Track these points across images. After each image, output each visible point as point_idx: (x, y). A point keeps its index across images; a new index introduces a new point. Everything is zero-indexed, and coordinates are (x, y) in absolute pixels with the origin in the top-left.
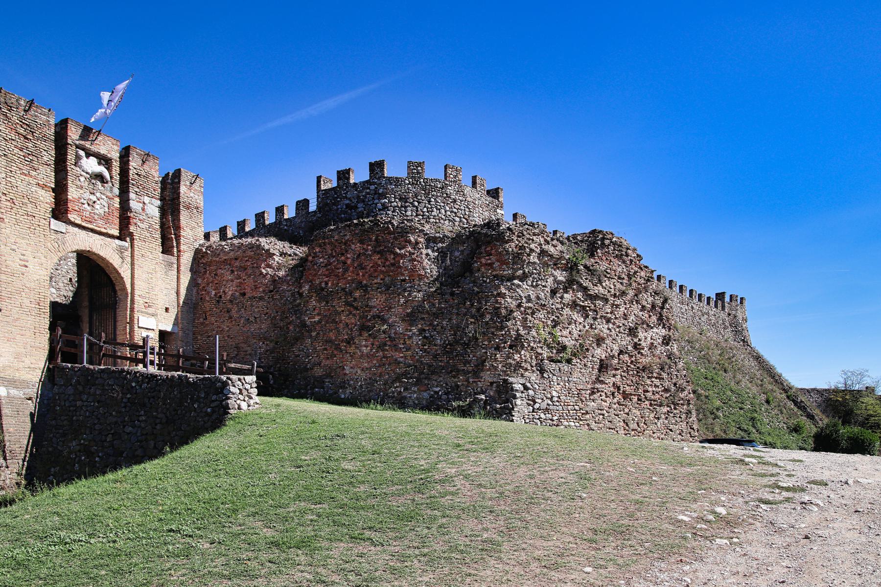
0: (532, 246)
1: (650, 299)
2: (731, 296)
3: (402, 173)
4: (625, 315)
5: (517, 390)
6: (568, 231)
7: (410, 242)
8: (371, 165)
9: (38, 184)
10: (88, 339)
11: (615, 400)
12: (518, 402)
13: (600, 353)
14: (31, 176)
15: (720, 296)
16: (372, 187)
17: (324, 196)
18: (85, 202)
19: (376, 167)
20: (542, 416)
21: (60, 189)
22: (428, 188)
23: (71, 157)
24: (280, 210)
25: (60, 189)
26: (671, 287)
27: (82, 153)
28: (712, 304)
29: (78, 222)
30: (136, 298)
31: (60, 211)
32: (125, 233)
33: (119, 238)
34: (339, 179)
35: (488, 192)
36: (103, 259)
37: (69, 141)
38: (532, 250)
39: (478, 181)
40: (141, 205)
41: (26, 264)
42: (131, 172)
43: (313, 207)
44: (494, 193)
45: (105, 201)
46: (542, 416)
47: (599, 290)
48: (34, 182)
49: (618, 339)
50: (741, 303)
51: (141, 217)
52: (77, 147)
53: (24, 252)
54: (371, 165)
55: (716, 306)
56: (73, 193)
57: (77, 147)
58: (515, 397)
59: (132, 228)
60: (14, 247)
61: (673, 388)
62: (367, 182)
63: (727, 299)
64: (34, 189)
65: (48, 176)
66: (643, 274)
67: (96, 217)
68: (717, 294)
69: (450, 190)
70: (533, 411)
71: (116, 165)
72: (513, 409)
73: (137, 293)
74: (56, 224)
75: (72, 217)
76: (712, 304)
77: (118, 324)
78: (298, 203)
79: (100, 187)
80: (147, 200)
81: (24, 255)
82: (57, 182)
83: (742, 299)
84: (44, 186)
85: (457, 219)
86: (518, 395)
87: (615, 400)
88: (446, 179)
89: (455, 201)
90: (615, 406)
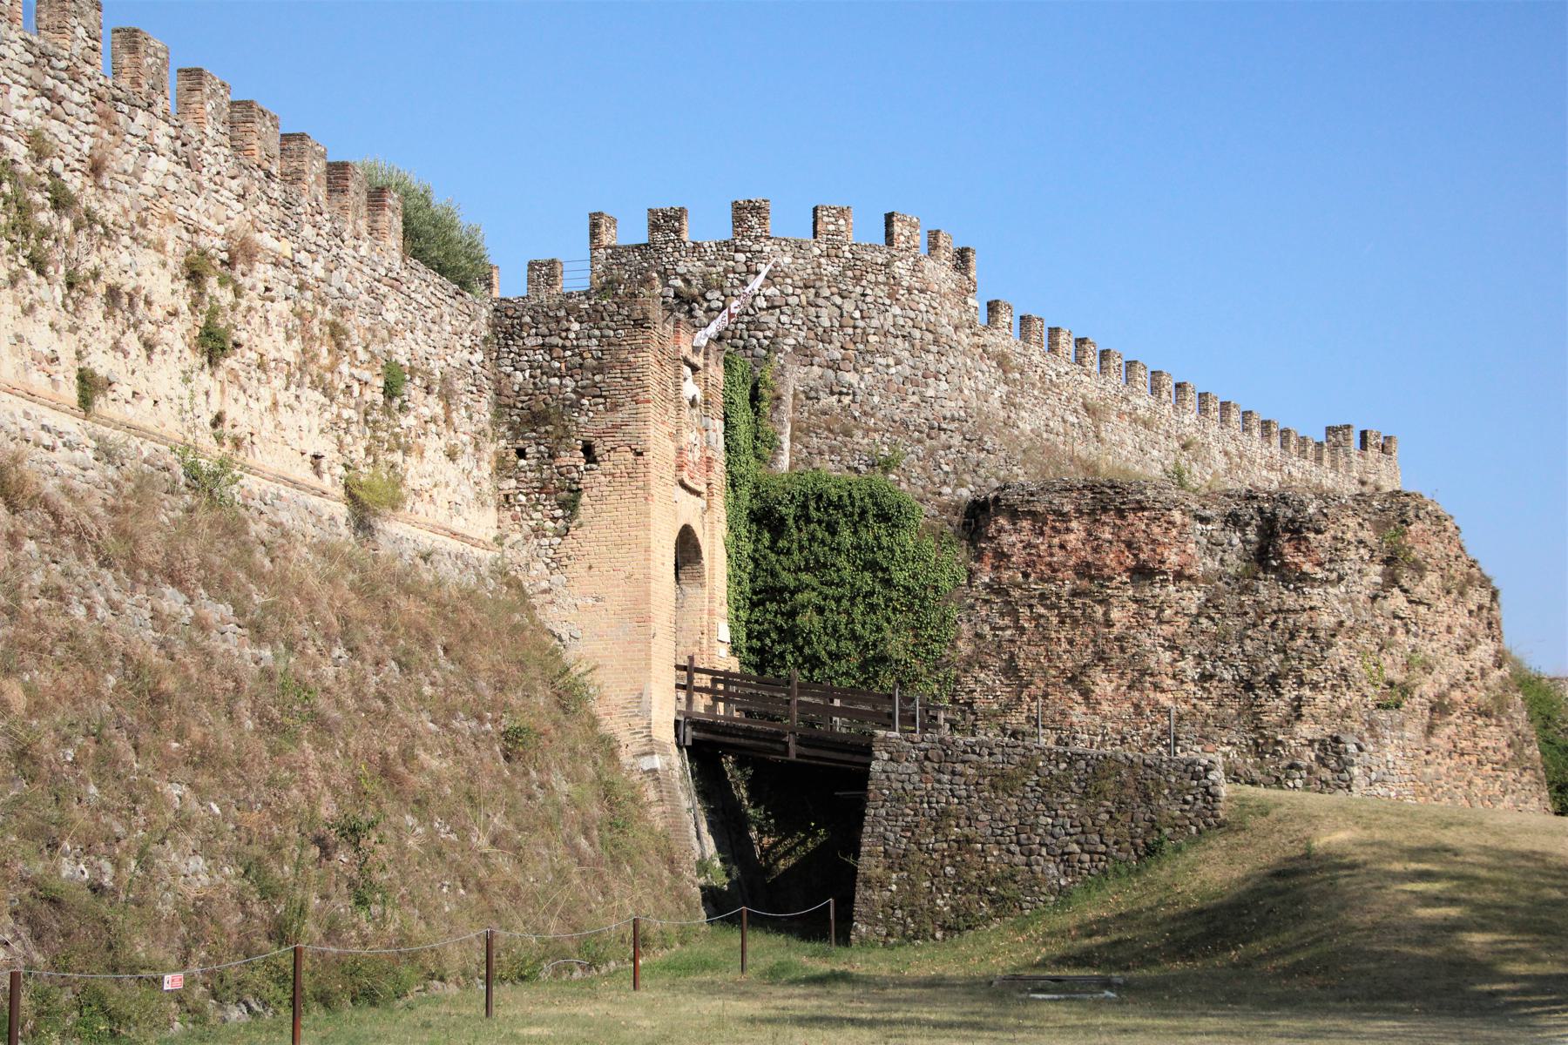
8: (737, 208)
12: (1355, 771)
13: (1428, 688)
16: (741, 257)
34: (654, 227)
44: (962, 258)
54: (737, 208)
62: (727, 244)
68: (1331, 430)
85: (917, 334)
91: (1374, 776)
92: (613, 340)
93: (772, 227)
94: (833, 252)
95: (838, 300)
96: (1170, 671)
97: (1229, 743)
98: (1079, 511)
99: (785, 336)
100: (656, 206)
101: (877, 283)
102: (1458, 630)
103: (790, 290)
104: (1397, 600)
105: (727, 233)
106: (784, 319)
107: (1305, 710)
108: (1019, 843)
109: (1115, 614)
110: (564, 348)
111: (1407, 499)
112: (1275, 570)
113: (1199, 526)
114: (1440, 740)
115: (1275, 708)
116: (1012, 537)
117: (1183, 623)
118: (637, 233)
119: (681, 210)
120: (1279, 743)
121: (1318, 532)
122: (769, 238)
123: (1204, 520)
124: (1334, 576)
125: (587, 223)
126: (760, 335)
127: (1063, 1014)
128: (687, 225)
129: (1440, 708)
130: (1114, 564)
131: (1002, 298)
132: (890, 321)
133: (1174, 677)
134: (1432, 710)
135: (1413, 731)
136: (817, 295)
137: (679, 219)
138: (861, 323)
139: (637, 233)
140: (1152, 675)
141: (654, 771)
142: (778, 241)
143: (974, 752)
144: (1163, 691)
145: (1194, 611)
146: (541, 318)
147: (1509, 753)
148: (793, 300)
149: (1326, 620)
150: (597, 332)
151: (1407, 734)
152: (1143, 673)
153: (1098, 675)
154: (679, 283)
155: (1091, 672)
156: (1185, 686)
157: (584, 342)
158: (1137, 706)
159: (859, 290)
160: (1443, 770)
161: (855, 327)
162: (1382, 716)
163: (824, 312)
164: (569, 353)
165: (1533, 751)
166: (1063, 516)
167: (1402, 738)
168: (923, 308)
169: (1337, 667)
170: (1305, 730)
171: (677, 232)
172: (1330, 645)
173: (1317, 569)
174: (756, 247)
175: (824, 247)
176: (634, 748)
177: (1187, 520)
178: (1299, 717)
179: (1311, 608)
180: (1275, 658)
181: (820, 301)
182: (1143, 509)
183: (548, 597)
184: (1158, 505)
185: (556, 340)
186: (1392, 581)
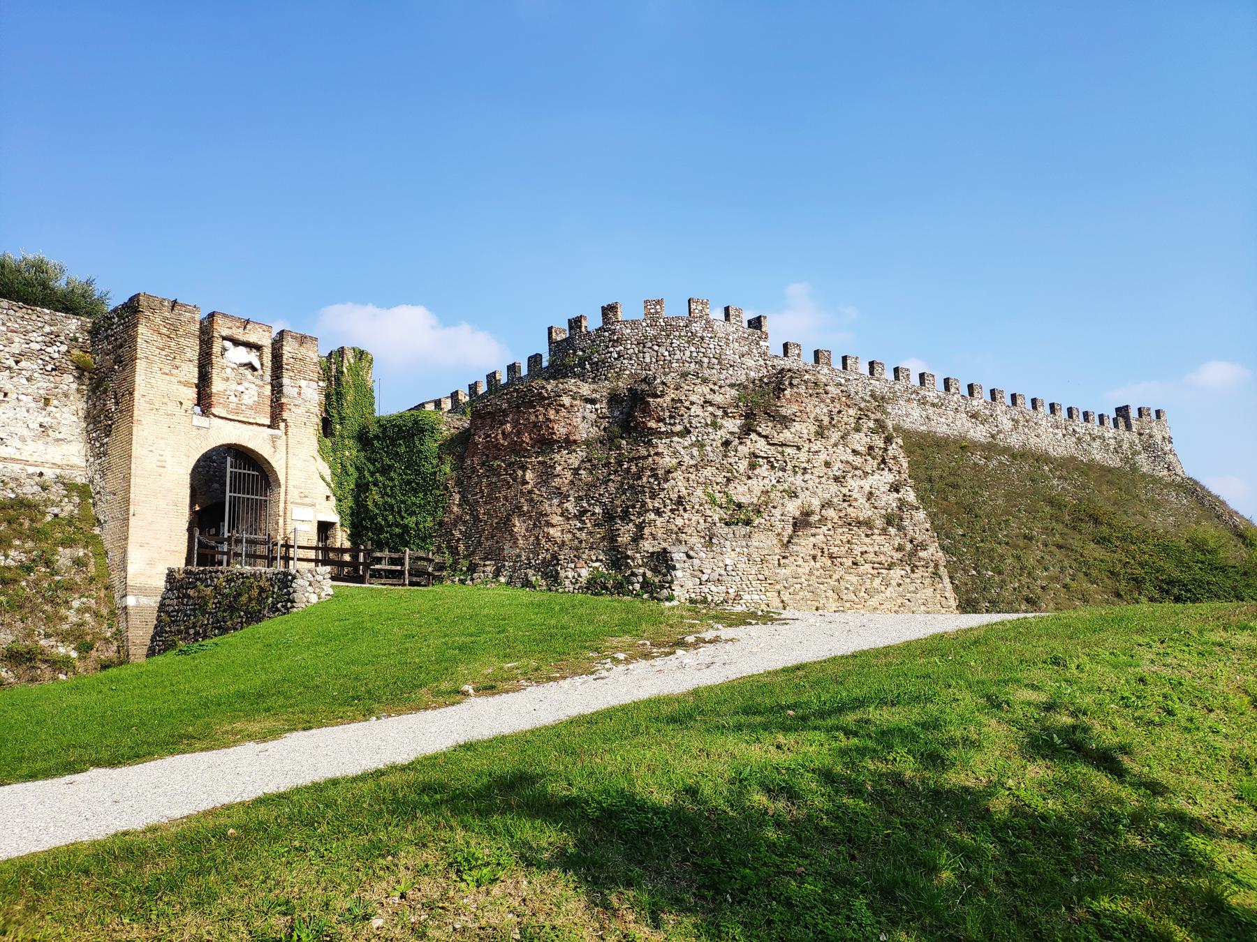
0: (693, 398)
1: (866, 440)
2: (1140, 409)
3: (639, 315)
7: (563, 406)
10: (200, 541)
11: (818, 565)
15: (1122, 412)
17: (557, 348)
19: (609, 311)
20: (713, 588)
22: (669, 328)
23: (216, 349)
26: (1034, 407)
27: (228, 344)
28: (1109, 423)
33: (269, 427)
34: (571, 328)
36: (253, 451)
37: (216, 334)
38: (692, 403)
39: (732, 312)
40: (297, 390)
42: (285, 357)
44: (756, 323)
45: (255, 391)
46: (713, 588)
47: (786, 435)
49: (819, 491)
50: (1158, 417)
52: (224, 338)
55: (1116, 426)
56: (217, 386)
57: (224, 338)
58: (674, 568)
59: (285, 415)
61: (909, 546)
63: (1133, 414)
64: (175, 387)
65: (192, 374)
66: (851, 412)
68: (1117, 410)
69: (696, 327)
71: (267, 353)
73: (291, 483)
74: (204, 421)
75: (214, 410)
76: (1109, 423)
78: (530, 359)
79: (250, 377)
80: (303, 383)
84: (186, 384)
85: (706, 360)
86: (678, 566)
87: (818, 565)
89: (702, 338)
90: (817, 573)
91: (705, 578)
93: (620, 316)
95: (656, 348)
96: (559, 511)
97: (597, 560)
107: (647, 531)
113: (589, 406)
114: (805, 544)
120: (628, 557)
121: (656, 396)
127: (381, 766)
128: (584, 323)
132: (688, 354)
133: (562, 515)
144: (553, 526)
153: (890, 529)
163: (647, 355)
172: (667, 480)
173: (661, 424)
182: (545, 398)
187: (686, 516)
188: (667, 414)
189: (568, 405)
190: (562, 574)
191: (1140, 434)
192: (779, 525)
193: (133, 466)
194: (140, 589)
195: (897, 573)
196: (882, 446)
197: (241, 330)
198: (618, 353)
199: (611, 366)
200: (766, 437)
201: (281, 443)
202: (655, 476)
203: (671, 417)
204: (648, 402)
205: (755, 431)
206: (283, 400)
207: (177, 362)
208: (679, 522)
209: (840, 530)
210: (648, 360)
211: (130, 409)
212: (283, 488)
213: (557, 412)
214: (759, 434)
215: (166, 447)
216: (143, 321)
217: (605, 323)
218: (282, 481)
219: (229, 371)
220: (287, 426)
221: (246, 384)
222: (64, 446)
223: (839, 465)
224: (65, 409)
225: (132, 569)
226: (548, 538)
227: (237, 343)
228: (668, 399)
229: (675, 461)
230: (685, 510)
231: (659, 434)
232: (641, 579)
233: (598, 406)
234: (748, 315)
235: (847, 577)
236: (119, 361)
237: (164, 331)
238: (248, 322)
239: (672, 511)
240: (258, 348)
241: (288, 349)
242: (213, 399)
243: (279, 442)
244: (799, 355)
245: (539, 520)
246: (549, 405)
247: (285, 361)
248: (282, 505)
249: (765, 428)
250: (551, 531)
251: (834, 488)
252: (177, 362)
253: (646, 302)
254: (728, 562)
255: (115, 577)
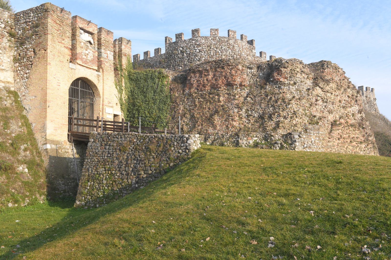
2: (366, 88)
3: (208, 34)
4: (340, 101)
5: (197, 134)
6: (307, 61)
7: (239, 69)
8: (193, 31)
9: (65, 47)
11: (340, 142)
12: (297, 144)
13: (331, 118)
14: (62, 43)
16: (194, 42)
18: (84, 54)
19: (195, 32)
21: (73, 48)
22: (221, 41)
24: (146, 53)
25: (73, 48)
27: (82, 31)
29: (81, 64)
30: (105, 99)
31: (73, 59)
32: (100, 67)
33: (97, 71)
34: (177, 38)
35: (248, 42)
39: (243, 37)
41: (60, 84)
43: (163, 51)
44: (251, 42)
47: (328, 88)
48: (63, 46)
51: (106, 60)
53: (59, 79)
54: (193, 31)
56: (79, 50)
58: (295, 141)
59: (103, 66)
60: (55, 77)
62: (191, 39)
63: (365, 89)
65: (68, 42)
67: (88, 61)
69: (231, 42)
70: (304, 148)
71: (96, 37)
72: (295, 147)
73: (105, 97)
74: (71, 65)
77: (95, 112)
80: (108, 52)
81: (59, 80)
82: (73, 45)
83: (372, 89)
84: (67, 48)
88: (229, 36)
91: (305, 146)
92: (40, 17)
94: (214, 39)
95: (215, 49)
97: (256, 137)
98: (211, 68)
99: (202, 57)
100: (177, 33)
101: (225, 45)
102: (343, 102)
103: (204, 47)
104: (318, 90)
105: (191, 37)
106: (202, 54)
107: (281, 125)
108: (125, 171)
109: (221, 99)
110: (29, 22)
111: (325, 62)
112: (272, 81)
113: (249, 70)
114: (335, 133)
115: (270, 125)
116: (194, 79)
117: (242, 99)
118: (174, 40)
119: (182, 33)
120: (272, 136)
121: (285, 68)
122: (199, 37)
123: (251, 68)
124: (292, 82)
125: (164, 39)
126: (197, 57)
129: (334, 124)
130: (221, 83)
131: (263, 51)
132: (228, 53)
134: (332, 125)
135: (324, 132)
136: (210, 48)
137: (181, 35)
138: (221, 54)
139: (174, 40)
140: (231, 116)
141: (46, 149)
142: (201, 37)
143: (116, 137)
145: (245, 95)
146: (25, 14)
147: (363, 139)
148: (205, 50)
149: (289, 96)
150: (37, 15)
151: (321, 132)
152: (229, 116)
154: (181, 49)
155: (213, 117)
156: (243, 120)
157: (34, 19)
158: (227, 126)
159: (220, 47)
160: (336, 144)
161: (219, 55)
162: (310, 127)
163: (212, 52)
164: (31, 23)
165: (372, 138)
166: (207, 71)
167: (318, 133)
168: (237, 50)
169: (292, 111)
170: (281, 132)
171: (181, 38)
172: (289, 104)
173: (285, 80)
174: (197, 39)
175: (212, 38)
176: (42, 142)
177: (244, 68)
178: (278, 127)
179: (283, 93)
180: (271, 109)
181: (211, 50)
182: (229, 66)
183: (24, 97)
184: (234, 64)
185: (28, 20)
186: (316, 84)
187: (297, 120)
188: (289, 76)
189: (241, 69)
190: (240, 141)
191: (366, 97)
192: (327, 125)
193: (48, 84)
194: (51, 141)
195: (363, 146)
196: (356, 95)
197: (86, 25)
198: (199, 50)
199: (196, 55)
200: (322, 88)
201: (101, 78)
202: (285, 102)
203: (290, 77)
204: (281, 71)
205: (318, 85)
206: (102, 59)
207: (64, 37)
208: (294, 122)
209: (346, 128)
210: (212, 54)
211: (45, 57)
212: (102, 98)
213: (236, 72)
214: (320, 87)
215: (58, 76)
216: (50, 16)
217: (194, 37)
218: (101, 95)
219: (82, 44)
220: (103, 70)
221: (89, 50)
222: (5, 73)
223: (343, 102)
224: (5, 55)
225: (48, 132)
226: (233, 126)
227: (86, 31)
228: (289, 69)
229: (291, 97)
230: (296, 117)
231: (284, 84)
232: (280, 145)
233: (252, 71)
234: (249, 39)
235: (349, 147)
236: (36, 33)
237: (58, 22)
238: (90, 22)
239: (291, 118)
240: (91, 34)
241: (103, 35)
242: (78, 55)
243: (100, 78)
244: (265, 57)
245: (229, 118)
246: (232, 69)
247: (102, 42)
248: (101, 106)
249: (321, 84)
250: (234, 123)
251: (342, 110)
252: (64, 37)
253: (211, 29)
254: (313, 139)
255: (38, 136)
